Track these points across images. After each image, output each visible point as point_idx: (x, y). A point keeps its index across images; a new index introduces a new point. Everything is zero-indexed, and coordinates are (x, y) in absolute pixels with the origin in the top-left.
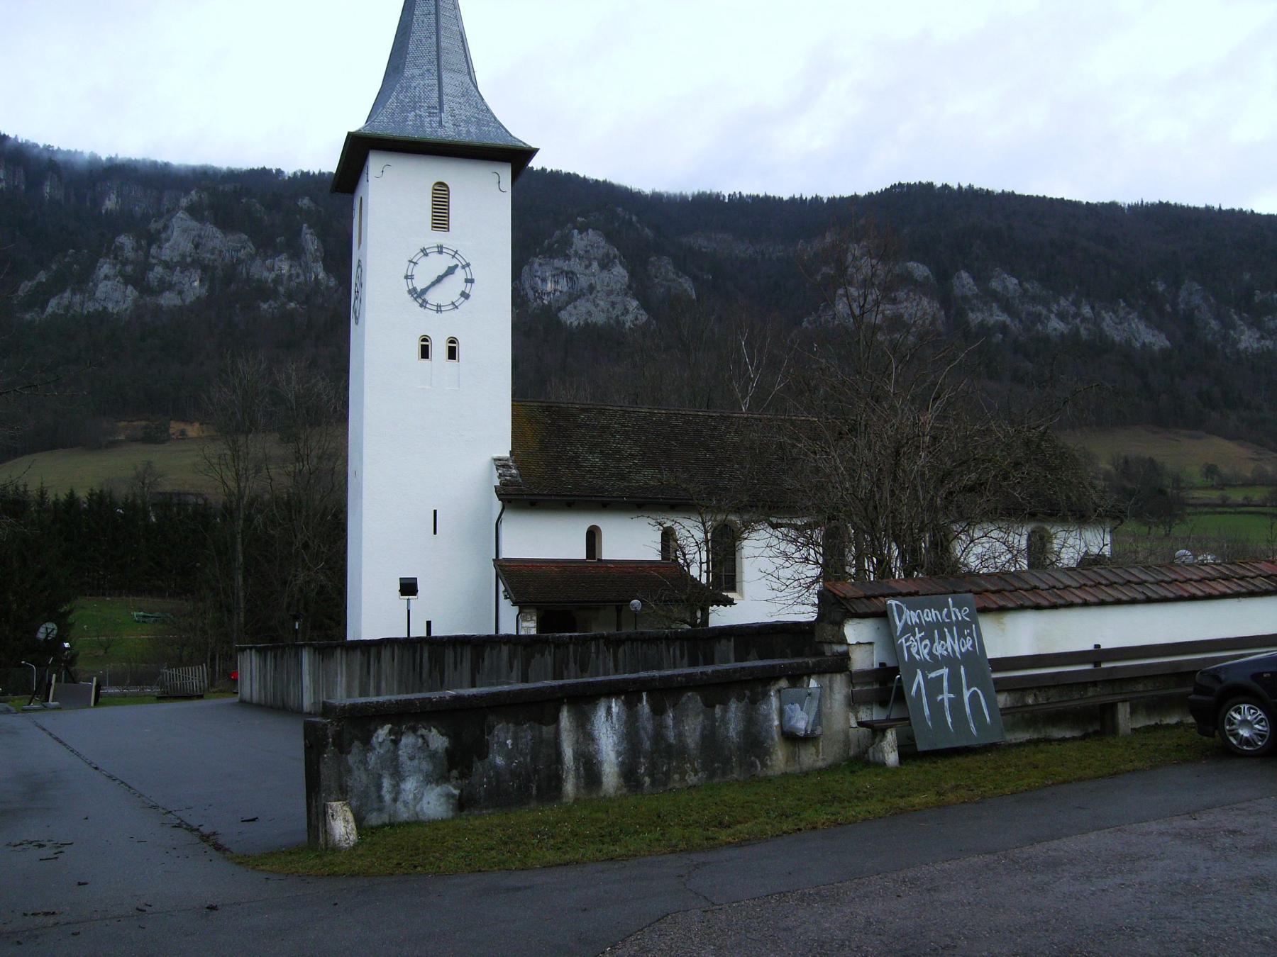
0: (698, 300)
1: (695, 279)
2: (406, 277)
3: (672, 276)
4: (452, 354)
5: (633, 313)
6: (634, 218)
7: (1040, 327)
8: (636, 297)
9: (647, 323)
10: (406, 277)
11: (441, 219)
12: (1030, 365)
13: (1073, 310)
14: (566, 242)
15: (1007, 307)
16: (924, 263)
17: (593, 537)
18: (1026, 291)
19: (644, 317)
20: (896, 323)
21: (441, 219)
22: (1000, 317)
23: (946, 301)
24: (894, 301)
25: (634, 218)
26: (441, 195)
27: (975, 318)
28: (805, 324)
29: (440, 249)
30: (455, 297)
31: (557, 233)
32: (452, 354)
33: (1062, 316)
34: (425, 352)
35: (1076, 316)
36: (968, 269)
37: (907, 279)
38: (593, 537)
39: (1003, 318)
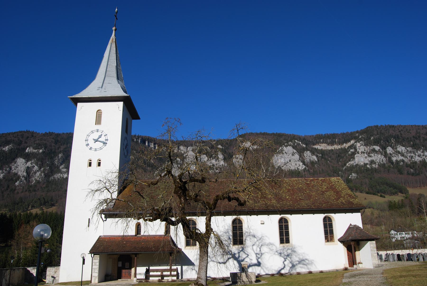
0: (318, 160)
1: (317, 156)
2: (86, 141)
3: (311, 156)
4: (99, 164)
5: (302, 167)
6: (300, 143)
7: (413, 160)
8: (301, 162)
9: (305, 168)
10: (86, 141)
11: (98, 121)
12: (412, 170)
13: (422, 154)
14: (282, 150)
15: (403, 155)
16: (377, 145)
17: (138, 226)
18: (408, 150)
19: (304, 167)
20: (372, 162)
21: (98, 121)
22: (400, 158)
23: (386, 155)
24: (371, 156)
25: (300, 143)
26: (99, 114)
27: (394, 159)
28: (347, 165)
29: (98, 131)
30: (89, 142)
31: (280, 148)
32: (99, 164)
33: (419, 156)
34: (90, 165)
35: (423, 156)
36: (391, 146)
37: (374, 151)
38: (138, 226)
39: (402, 158)
